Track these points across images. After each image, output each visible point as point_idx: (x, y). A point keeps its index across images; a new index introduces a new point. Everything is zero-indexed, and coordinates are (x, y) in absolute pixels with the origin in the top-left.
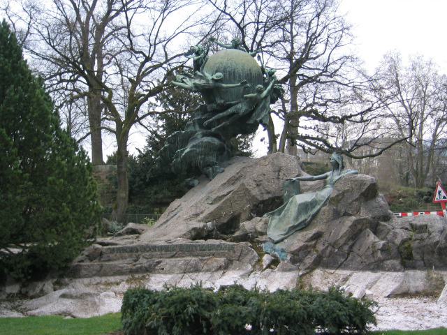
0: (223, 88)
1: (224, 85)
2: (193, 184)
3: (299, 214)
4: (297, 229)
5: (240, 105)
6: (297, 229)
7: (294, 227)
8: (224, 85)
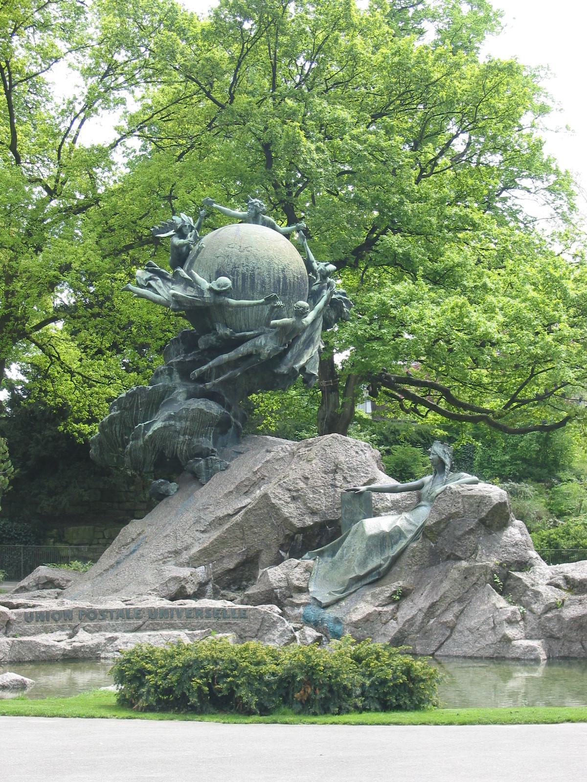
0: (229, 305)
1: (233, 301)
2: (167, 491)
5: (261, 340)
7: (359, 579)
8: (233, 301)
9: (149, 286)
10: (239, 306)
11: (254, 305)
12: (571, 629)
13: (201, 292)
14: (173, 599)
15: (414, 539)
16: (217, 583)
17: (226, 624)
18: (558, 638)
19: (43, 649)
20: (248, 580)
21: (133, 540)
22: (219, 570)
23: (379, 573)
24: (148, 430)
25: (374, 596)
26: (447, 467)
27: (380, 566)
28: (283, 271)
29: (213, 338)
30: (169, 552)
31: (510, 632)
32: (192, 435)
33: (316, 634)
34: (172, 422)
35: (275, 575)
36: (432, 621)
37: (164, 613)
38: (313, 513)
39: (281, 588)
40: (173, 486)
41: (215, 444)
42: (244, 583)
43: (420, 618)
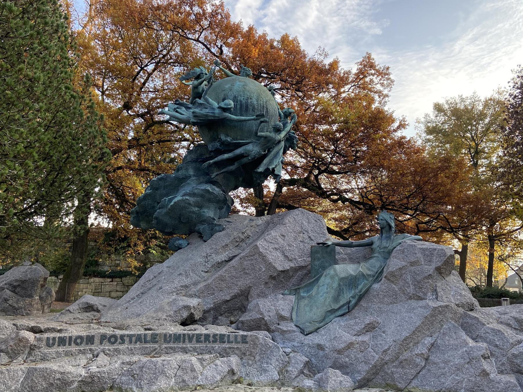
3: (339, 292)
4: (340, 313)
5: (250, 147)
7: (333, 311)
9: (177, 112)
14: (184, 323)
17: (230, 348)
19: (58, 376)
21: (155, 277)
24: (171, 202)
26: (393, 229)
28: (266, 102)
30: (182, 286)
31: (486, 366)
34: (187, 197)
37: (177, 338)
41: (215, 214)
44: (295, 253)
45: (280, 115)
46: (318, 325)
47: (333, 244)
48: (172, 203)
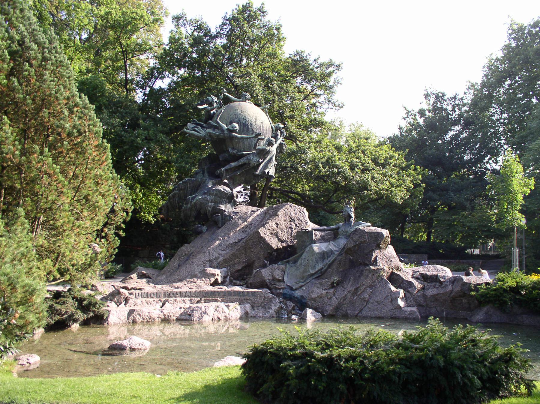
6: (313, 277)
9: (194, 130)
10: (242, 138)
11: (247, 138)
12: (431, 301)
13: (223, 131)
15: (340, 254)
16: (232, 277)
18: (423, 306)
20: (247, 275)
22: (233, 270)
23: (321, 272)
25: (321, 284)
27: (322, 268)
29: (227, 155)
32: (215, 203)
33: (293, 305)
35: (266, 273)
36: (355, 298)
38: (282, 241)
39: (269, 279)
40: (205, 228)
42: (245, 277)
43: (349, 295)
44: (284, 236)
45: (272, 128)
46: (302, 284)
47: (313, 229)
48: (195, 201)
